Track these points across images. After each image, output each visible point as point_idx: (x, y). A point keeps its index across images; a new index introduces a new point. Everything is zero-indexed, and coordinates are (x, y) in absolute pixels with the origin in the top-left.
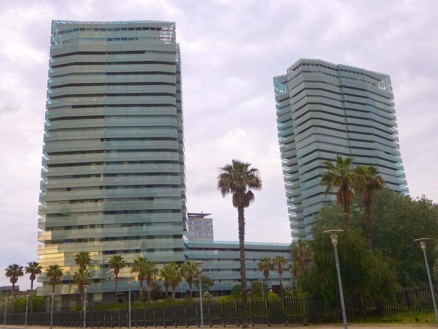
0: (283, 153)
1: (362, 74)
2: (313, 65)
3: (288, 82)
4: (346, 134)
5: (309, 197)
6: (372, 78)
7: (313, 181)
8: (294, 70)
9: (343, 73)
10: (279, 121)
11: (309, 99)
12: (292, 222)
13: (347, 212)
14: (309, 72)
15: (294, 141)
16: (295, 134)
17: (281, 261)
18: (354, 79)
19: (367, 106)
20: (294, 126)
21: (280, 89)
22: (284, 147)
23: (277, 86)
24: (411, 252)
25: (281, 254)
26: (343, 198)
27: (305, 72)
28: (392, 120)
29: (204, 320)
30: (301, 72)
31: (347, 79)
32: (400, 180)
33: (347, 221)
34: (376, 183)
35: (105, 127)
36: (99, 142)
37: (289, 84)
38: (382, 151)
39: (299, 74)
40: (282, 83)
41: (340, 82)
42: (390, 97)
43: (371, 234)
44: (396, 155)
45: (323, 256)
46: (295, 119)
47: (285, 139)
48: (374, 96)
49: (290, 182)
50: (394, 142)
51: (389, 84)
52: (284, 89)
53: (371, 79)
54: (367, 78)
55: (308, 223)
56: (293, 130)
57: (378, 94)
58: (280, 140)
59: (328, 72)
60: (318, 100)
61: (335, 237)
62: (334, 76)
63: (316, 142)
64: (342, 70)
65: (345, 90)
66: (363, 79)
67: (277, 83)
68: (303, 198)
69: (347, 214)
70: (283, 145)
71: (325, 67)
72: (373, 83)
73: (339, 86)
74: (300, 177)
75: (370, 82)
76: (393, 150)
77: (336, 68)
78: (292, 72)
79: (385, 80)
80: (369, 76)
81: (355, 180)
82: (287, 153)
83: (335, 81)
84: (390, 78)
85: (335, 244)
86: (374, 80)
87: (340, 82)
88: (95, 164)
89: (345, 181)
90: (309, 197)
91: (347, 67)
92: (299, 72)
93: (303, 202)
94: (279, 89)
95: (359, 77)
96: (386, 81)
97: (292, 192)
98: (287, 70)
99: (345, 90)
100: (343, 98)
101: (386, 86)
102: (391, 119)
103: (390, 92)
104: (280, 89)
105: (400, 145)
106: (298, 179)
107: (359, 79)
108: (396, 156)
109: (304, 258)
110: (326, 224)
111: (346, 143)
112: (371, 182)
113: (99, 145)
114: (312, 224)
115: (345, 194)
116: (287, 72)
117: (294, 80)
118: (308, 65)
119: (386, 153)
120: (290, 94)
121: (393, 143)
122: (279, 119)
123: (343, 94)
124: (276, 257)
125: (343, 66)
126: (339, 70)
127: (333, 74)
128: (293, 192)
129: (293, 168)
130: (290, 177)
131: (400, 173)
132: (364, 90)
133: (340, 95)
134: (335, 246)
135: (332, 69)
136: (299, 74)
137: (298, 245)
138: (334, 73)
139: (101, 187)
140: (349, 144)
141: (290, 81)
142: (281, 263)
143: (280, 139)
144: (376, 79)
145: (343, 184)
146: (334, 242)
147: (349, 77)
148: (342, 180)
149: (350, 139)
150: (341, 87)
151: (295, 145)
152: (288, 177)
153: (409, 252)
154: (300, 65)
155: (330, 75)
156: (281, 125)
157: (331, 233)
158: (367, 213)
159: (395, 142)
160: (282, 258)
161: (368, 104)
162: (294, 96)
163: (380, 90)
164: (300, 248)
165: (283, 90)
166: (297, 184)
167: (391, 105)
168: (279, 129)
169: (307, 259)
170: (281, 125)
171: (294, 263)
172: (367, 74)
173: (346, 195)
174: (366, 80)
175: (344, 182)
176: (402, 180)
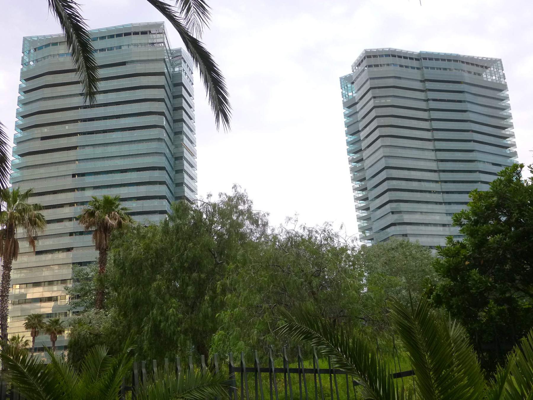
2: (381, 56)
4: (431, 143)
7: (383, 209)
10: (347, 134)
11: (376, 101)
14: (377, 66)
18: (445, 69)
22: (355, 166)
31: (432, 70)
35: (77, 160)
36: (70, 179)
42: (503, 88)
53: (465, 65)
60: (389, 101)
62: (413, 68)
65: (429, 85)
73: (421, 81)
83: (416, 73)
84: (501, 62)
87: (423, 75)
88: (69, 205)
91: (432, 54)
95: (452, 65)
99: (429, 85)
105: (518, 153)
111: (431, 155)
113: (70, 183)
125: (427, 53)
135: (411, 59)
138: (415, 64)
139: (71, 234)
154: (365, 58)
168: (349, 143)
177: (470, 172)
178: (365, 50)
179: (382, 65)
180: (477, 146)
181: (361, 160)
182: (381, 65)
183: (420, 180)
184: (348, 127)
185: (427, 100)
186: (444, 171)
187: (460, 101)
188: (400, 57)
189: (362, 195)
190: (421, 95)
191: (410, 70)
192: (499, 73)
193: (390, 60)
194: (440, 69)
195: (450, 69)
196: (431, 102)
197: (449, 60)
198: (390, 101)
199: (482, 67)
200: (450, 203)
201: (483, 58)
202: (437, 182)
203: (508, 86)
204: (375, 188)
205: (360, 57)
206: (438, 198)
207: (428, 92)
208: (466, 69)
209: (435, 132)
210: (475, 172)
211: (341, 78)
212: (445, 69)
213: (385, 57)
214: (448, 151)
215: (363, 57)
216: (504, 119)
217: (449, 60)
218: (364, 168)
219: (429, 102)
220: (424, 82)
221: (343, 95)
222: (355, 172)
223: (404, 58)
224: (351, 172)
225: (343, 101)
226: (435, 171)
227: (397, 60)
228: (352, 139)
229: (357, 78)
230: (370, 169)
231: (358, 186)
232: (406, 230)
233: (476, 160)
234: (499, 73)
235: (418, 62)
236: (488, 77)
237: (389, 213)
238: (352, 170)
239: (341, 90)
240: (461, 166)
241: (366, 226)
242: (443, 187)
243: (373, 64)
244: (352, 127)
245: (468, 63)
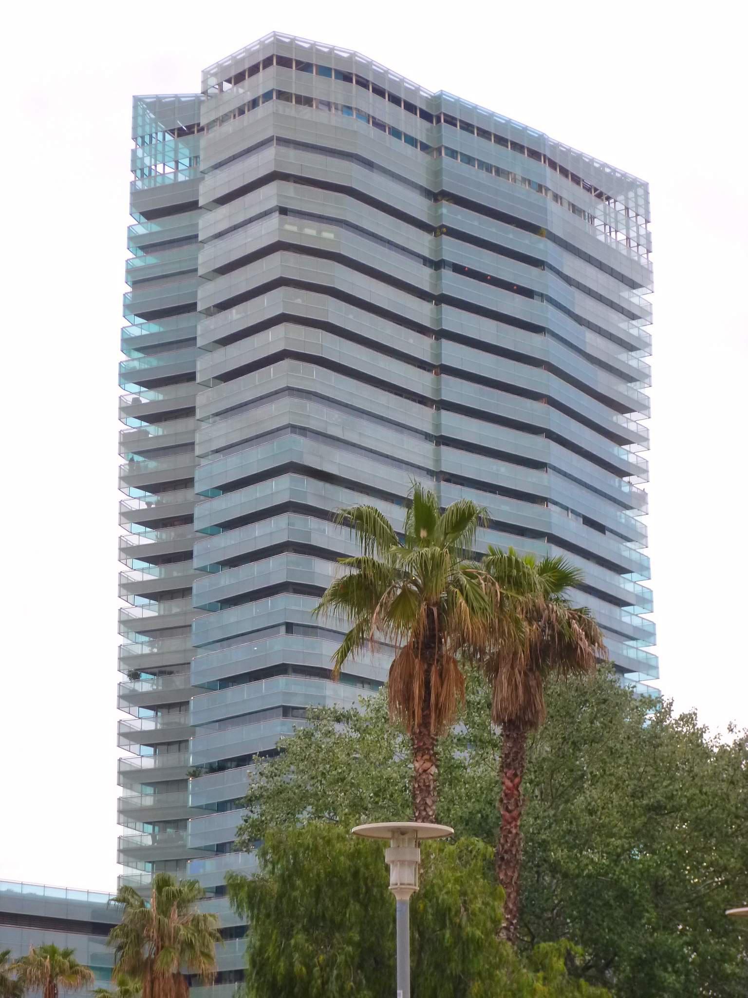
0: (132, 460)
1: (535, 154)
2: (325, 71)
3: (201, 130)
4: (428, 412)
5: (226, 682)
6: (576, 180)
7: (252, 609)
8: (239, 78)
9: (452, 137)
10: (131, 308)
11: (288, 227)
12: (131, 789)
13: (426, 757)
15: (189, 412)
16: (199, 379)
17: (62, 972)
18: (499, 172)
19: (536, 302)
20: (200, 342)
21: (160, 157)
22: (142, 433)
23: (147, 139)
24: (676, 972)
25: (59, 940)
26: (417, 689)
27: (283, 96)
28: (631, 382)
30: (267, 96)
31: (465, 166)
32: (632, 654)
33: (423, 799)
34: (567, 639)
37: (204, 140)
38: (573, 512)
39: (254, 103)
40: (172, 132)
41: (437, 174)
43: (514, 872)
44: (629, 540)
45: (296, 956)
46: (208, 309)
47: (148, 397)
48: (571, 266)
49: (146, 601)
50: (626, 479)
51: (641, 220)
52: (177, 162)
53: (569, 182)
54: (552, 179)
55: (203, 802)
56: (195, 362)
57: (589, 259)
58: (126, 397)
59: (387, 120)
61: (408, 857)
62: (411, 141)
63: (291, 432)
64: (451, 121)
66: (535, 180)
67: (147, 128)
68: (195, 681)
69: (427, 765)
70: (137, 423)
71: (379, 92)
72: (574, 206)
74: (197, 587)
75: (561, 198)
76: (619, 513)
77: (424, 108)
78: (227, 86)
79: (627, 199)
80: (564, 172)
81: (484, 610)
82: (152, 465)
84: (647, 193)
85: (402, 891)
86: (579, 191)
87: (437, 174)
89: (435, 610)
90: (226, 682)
92: (261, 92)
93: (192, 703)
94: (156, 155)
95: (519, 164)
96: (631, 204)
97: (146, 650)
98: (206, 74)
100: (438, 249)
101: (628, 229)
102: (629, 379)
103: (640, 256)
104: (160, 157)
105: (650, 499)
106: (185, 592)
107: (519, 178)
108: (629, 544)
109: (173, 969)
110: (309, 808)
112: (544, 631)
114: (249, 801)
115: (427, 672)
116: (204, 82)
117: (229, 127)
118: (304, 67)
119: (589, 522)
120: (202, 189)
121: (620, 486)
122: (134, 297)
123: (442, 233)
124: (38, 952)
125: (458, 103)
126: (439, 121)
128: (155, 650)
129: (167, 535)
130: (148, 577)
131: (636, 622)
132: (533, 229)
133: (426, 234)
134: (403, 903)
135: (410, 108)
136: (254, 103)
137: (151, 906)
138: (417, 127)
140: (438, 461)
141: (208, 129)
142: (60, 982)
143: (123, 393)
144: (589, 189)
145: (424, 620)
146: (401, 884)
147: (474, 159)
148: (423, 606)
149: (443, 441)
150: (437, 196)
151: (194, 431)
152: (137, 577)
153: (666, 970)
154: (268, 62)
155: (396, 133)
156: (141, 329)
157: (389, 835)
158: (510, 773)
159: (633, 479)
160: (66, 954)
161: (542, 296)
162: (223, 200)
163: (600, 241)
164: (161, 917)
165: (173, 164)
166: (176, 615)
167: (637, 312)
168: (129, 343)
169: (185, 972)
170: (141, 329)
171: (122, 983)
172: (557, 160)
173: (434, 678)
174: (549, 185)
175: (430, 613)
176: (640, 652)
177: (518, 534)
178: (275, 34)
180: (556, 454)
185: (437, 265)
187: (528, 293)
190: (422, 243)
191: (400, 145)
193: (336, 91)
196: (447, 274)
198: (331, 236)
203: (656, 276)
205: (250, 53)
207: (445, 238)
208: (564, 194)
221: (137, 167)
222: (139, 453)
224: (123, 450)
225: (133, 184)
232: (324, 697)
235: (426, 124)
238: (127, 442)
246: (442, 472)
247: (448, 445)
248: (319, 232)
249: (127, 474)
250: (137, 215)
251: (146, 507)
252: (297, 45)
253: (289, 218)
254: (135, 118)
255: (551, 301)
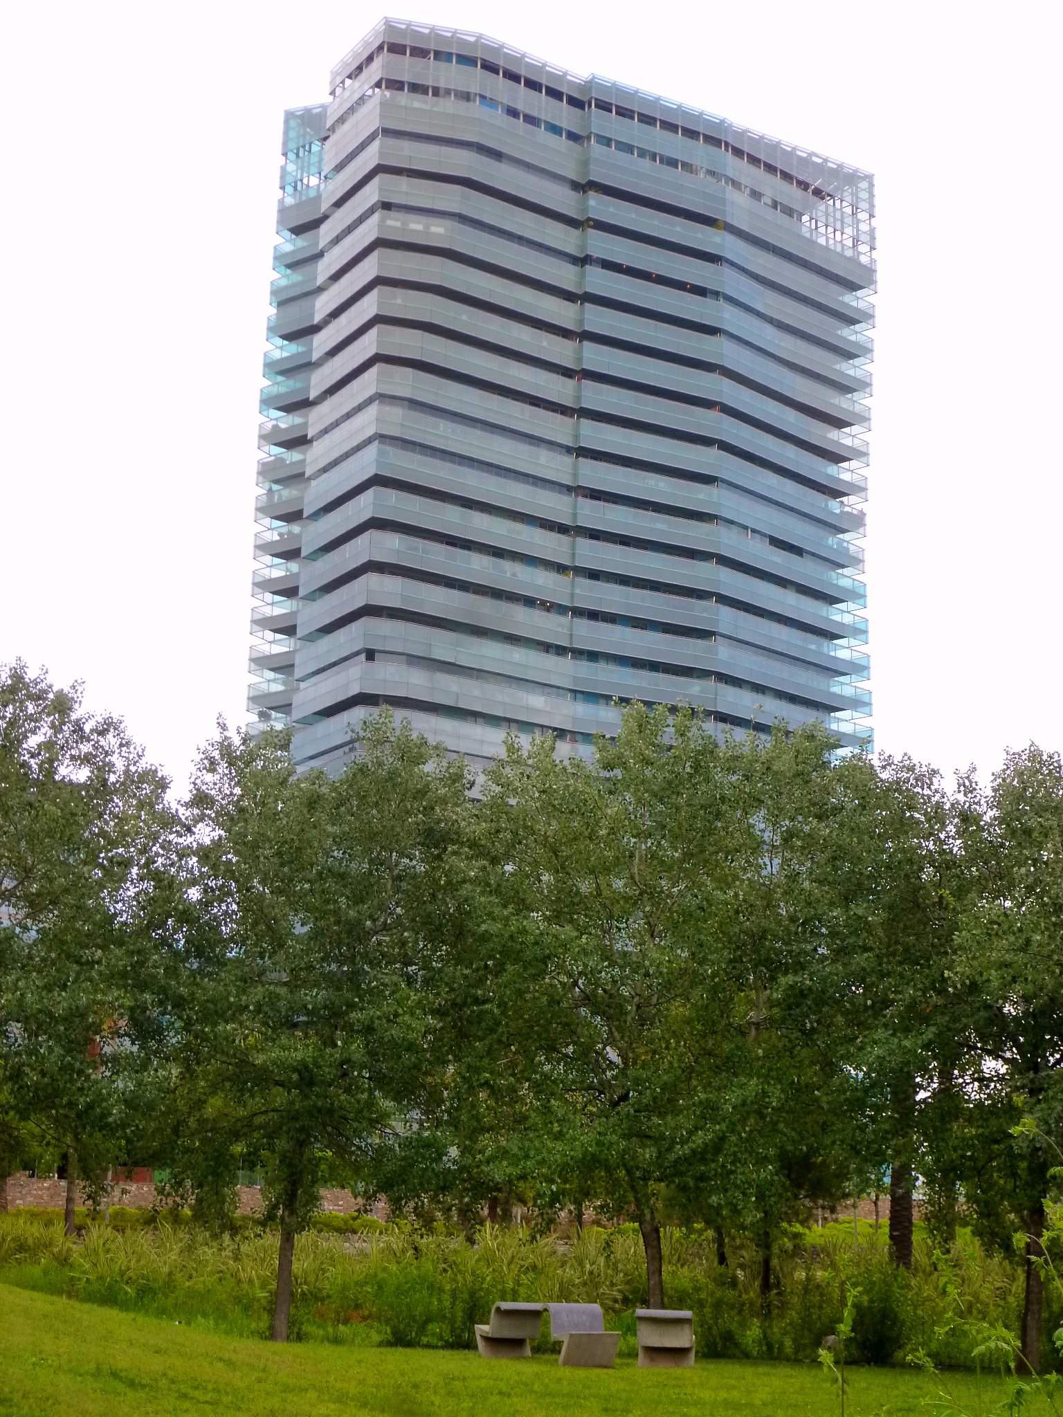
11: (390, 223)
18: (672, 163)
19: (709, 301)
21: (306, 169)
22: (279, 460)
29: (514, 1300)
41: (585, 163)
44: (843, 566)
53: (744, 164)
62: (554, 129)
65: (600, 207)
73: (576, 186)
84: (871, 185)
87: (585, 163)
95: (698, 153)
99: (600, 207)
105: (868, 520)
111: (557, 467)
125: (616, 89)
126: (590, 106)
127: (528, 111)
135: (554, 94)
138: (564, 115)
154: (380, 48)
163: (821, 245)
179: (442, 92)
181: (298, 441)
182: (436, 92)
183: (498, 553)
184: (280, 304)
185: (583, 261)
186: (595, 535)
187: (701, 291)
188: (513, 77)
189: (283, 574)
192: (858, 221)
193: (475, 79)
194: (653, 157)
195: (687, 167)
197: (691, 134)
198: (441, 230)
199: (804, 185)
200: (593, 656)
201: (794, 149)
202: (561, 569)
203: (880, 276)
204: (329, 552)
206: (553, 627)
208: (743, 181)
209: (587, 384)
210: (704, 560)
211: (289, 116)
212: (672, 163)
213: (457, 62)
214: (623, 465)
215: (377, 44)
216: (845, 388)
217: (691, 134)
218: (303, 474)
219: (587, 267)
220: (585, 192)
222: (276, 482)
223: (504, 76)
225: (281, 201)
226: (562, 529)
227: (499, 87)
228: (285, 354)
229: (342, 120)
230: (325, 476)
231: (277, 538)
233: (716, 517)
234: (858, 221)
236: (844, 242)
237: (357, 653)
238: (267, 471)
239: (281, 160)
240: (659, 526)
241: (276, 693)
242: (577, 591)
243: (406, 78)
244: (293, 309)
245: (754, 160)
246: (579, 487)
247: (586, 457)
248: (427, 227)
249: (264, 505)
250: (287, 234)
251: (278, 538)
252: (412, 30)
253: (392, 214)
254: (286, 133)
255: (730, 299)
